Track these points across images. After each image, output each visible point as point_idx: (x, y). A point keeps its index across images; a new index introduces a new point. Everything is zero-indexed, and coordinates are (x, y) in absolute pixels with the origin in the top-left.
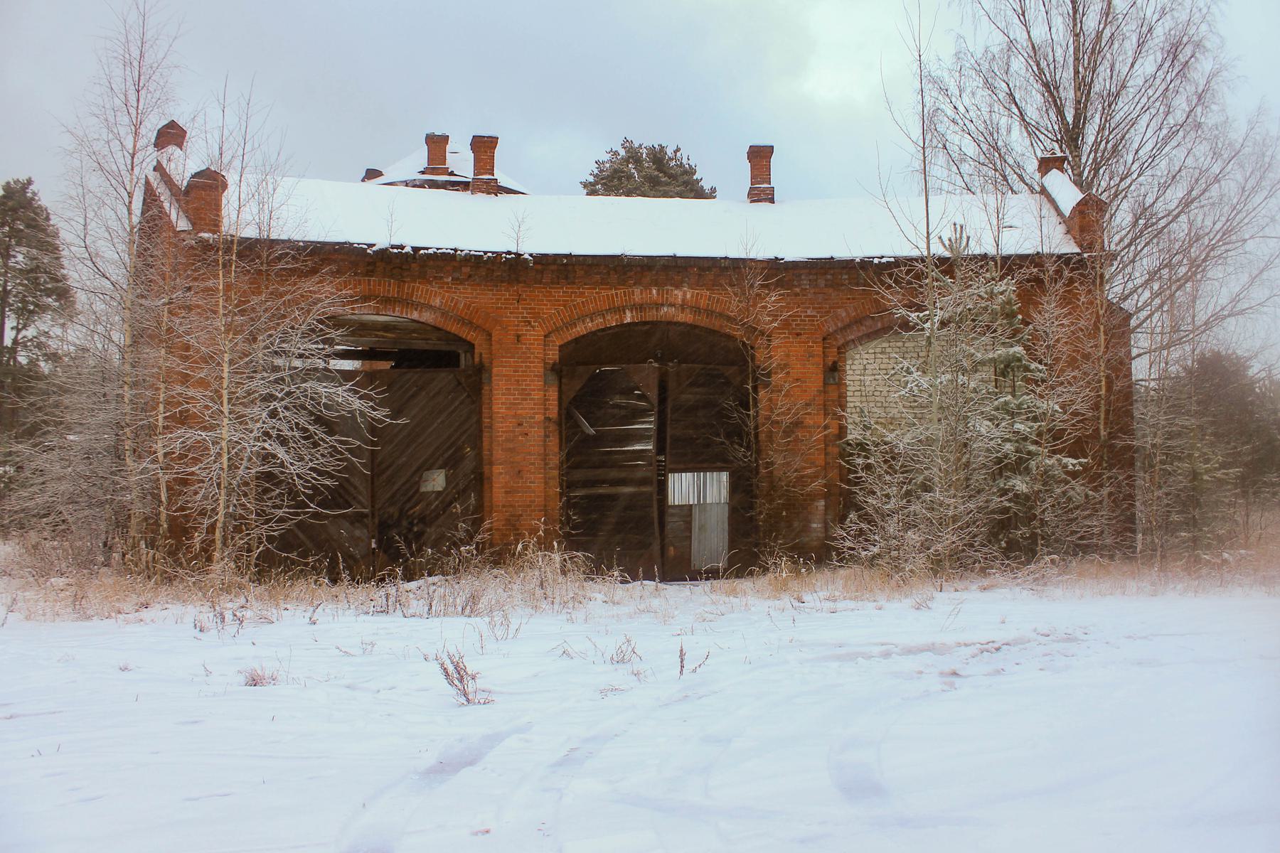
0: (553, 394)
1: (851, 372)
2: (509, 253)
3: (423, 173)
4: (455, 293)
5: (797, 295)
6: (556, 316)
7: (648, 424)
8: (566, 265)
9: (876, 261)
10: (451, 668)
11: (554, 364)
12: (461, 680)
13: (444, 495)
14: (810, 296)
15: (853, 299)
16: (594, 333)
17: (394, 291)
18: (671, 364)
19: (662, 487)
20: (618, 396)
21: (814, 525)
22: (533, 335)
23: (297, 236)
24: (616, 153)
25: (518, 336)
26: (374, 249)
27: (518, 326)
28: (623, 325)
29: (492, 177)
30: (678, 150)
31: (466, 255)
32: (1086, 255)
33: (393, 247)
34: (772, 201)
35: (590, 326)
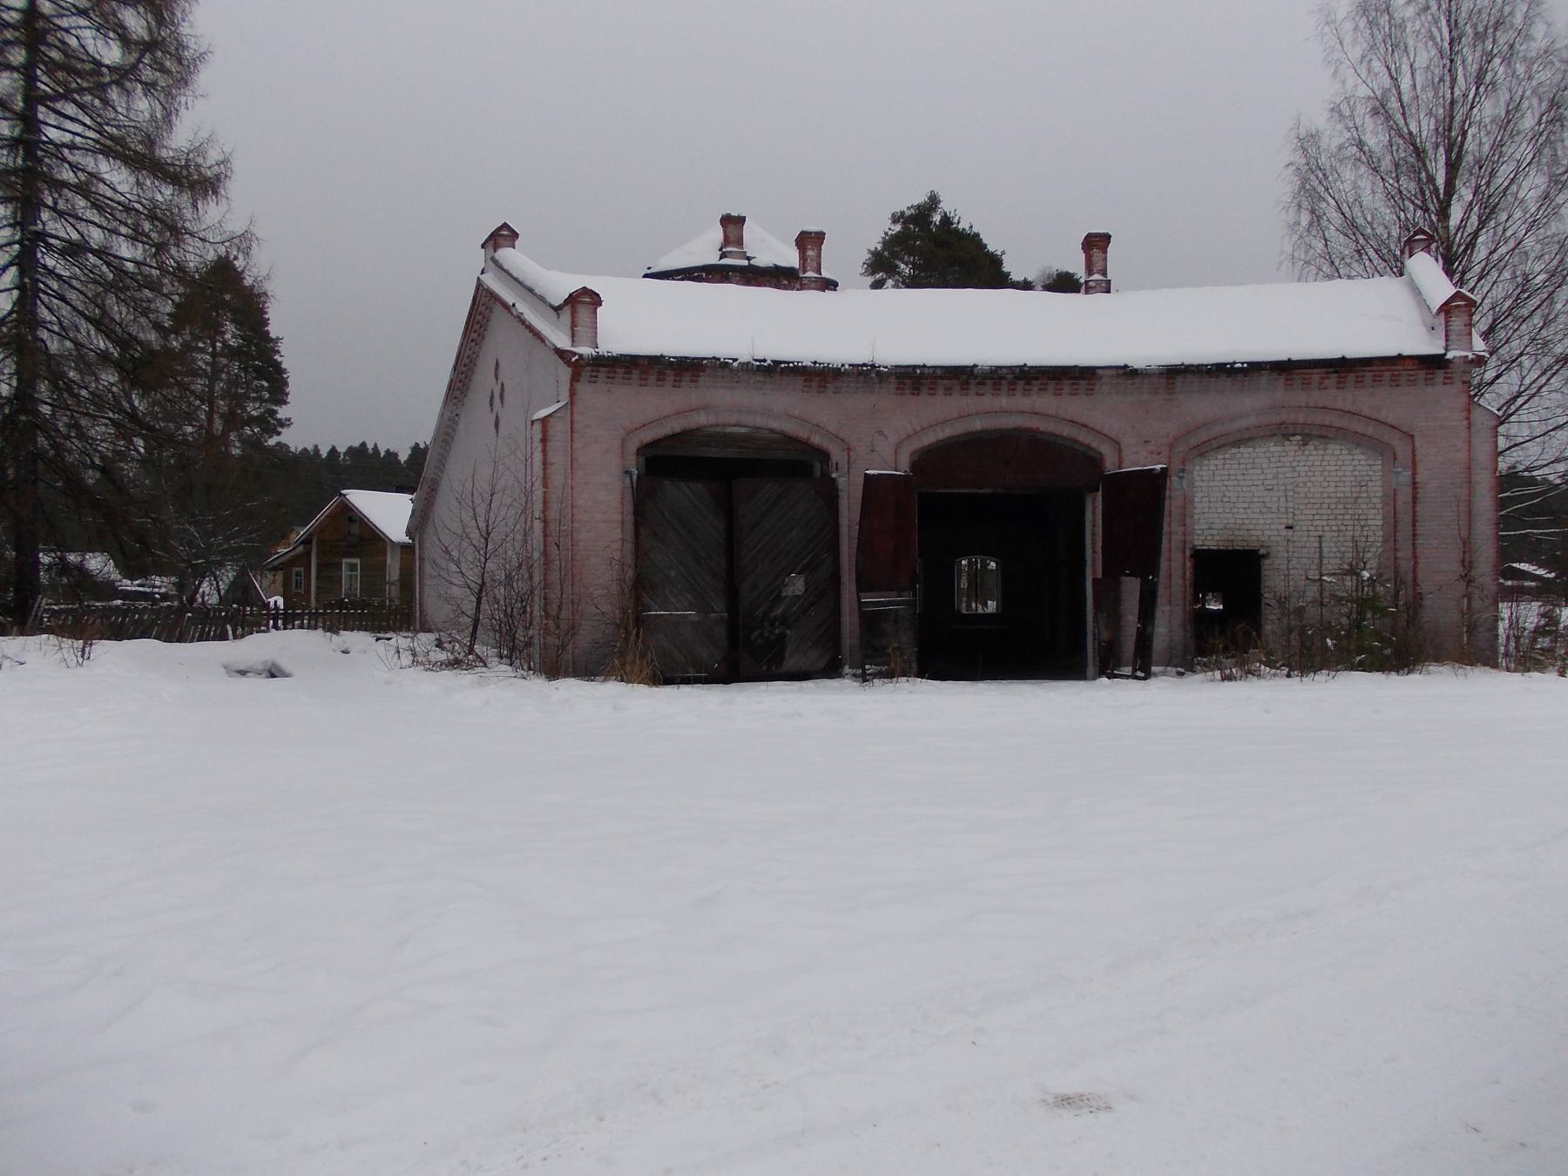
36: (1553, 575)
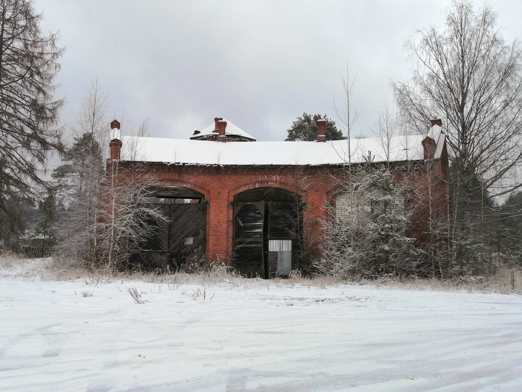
0: (231, 212)
2: (215, 165)
3: (214, 132)
4: (198, 178)
5: (317, 177)
7: (260, 223)
8: (235, 168)
10: (133, 292)
11: (232, 202)
12: (137, 296)
13: (192, 246)
14: (322, 178)
16: (246, 191)
17: (177, 177)
18: (270, 202)
19: (266, 246)
20: (252, 213)
23: (144, 160)
24: (300, 119)
25: (219, 192)
26: (170, 164)
27: (219, 189)
30: (326, 116)
31: (201, 165)
32: (425, 161)
33: (176, 163)
35: (244, 189)
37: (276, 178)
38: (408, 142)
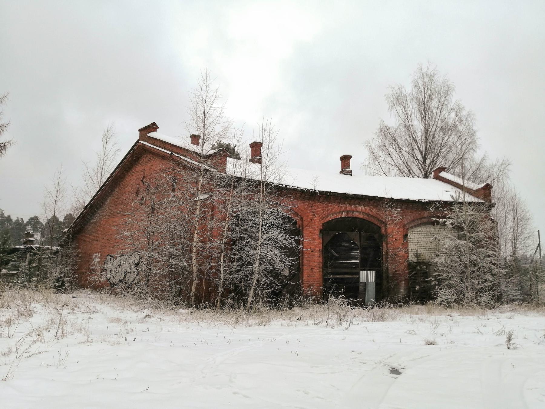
1: (410, 238)
2: (312, 190)
6: (323, 213)
9: (423, 201)
15: (413, 213)
21: (401, 290)
22: (316, 218)
28: (342, 218)
29: (349, 169)
34: (351, 175)
35: (332, 217)
36: (5, 223)
37: (362, 208)
38: (269, 163)
